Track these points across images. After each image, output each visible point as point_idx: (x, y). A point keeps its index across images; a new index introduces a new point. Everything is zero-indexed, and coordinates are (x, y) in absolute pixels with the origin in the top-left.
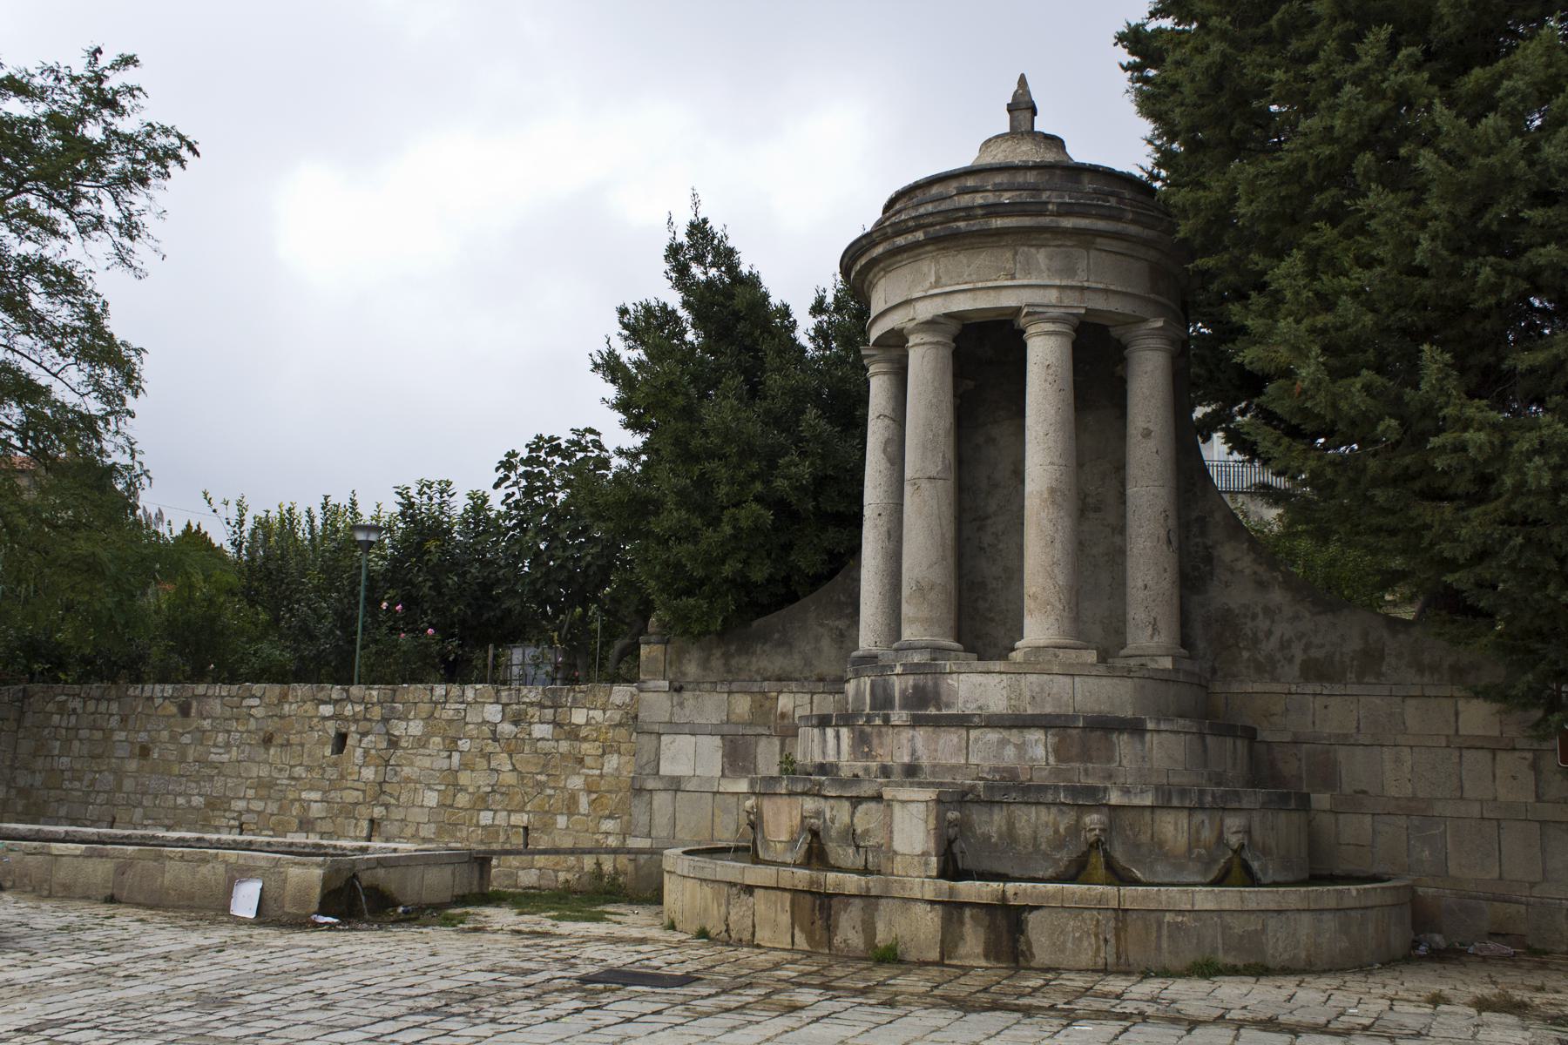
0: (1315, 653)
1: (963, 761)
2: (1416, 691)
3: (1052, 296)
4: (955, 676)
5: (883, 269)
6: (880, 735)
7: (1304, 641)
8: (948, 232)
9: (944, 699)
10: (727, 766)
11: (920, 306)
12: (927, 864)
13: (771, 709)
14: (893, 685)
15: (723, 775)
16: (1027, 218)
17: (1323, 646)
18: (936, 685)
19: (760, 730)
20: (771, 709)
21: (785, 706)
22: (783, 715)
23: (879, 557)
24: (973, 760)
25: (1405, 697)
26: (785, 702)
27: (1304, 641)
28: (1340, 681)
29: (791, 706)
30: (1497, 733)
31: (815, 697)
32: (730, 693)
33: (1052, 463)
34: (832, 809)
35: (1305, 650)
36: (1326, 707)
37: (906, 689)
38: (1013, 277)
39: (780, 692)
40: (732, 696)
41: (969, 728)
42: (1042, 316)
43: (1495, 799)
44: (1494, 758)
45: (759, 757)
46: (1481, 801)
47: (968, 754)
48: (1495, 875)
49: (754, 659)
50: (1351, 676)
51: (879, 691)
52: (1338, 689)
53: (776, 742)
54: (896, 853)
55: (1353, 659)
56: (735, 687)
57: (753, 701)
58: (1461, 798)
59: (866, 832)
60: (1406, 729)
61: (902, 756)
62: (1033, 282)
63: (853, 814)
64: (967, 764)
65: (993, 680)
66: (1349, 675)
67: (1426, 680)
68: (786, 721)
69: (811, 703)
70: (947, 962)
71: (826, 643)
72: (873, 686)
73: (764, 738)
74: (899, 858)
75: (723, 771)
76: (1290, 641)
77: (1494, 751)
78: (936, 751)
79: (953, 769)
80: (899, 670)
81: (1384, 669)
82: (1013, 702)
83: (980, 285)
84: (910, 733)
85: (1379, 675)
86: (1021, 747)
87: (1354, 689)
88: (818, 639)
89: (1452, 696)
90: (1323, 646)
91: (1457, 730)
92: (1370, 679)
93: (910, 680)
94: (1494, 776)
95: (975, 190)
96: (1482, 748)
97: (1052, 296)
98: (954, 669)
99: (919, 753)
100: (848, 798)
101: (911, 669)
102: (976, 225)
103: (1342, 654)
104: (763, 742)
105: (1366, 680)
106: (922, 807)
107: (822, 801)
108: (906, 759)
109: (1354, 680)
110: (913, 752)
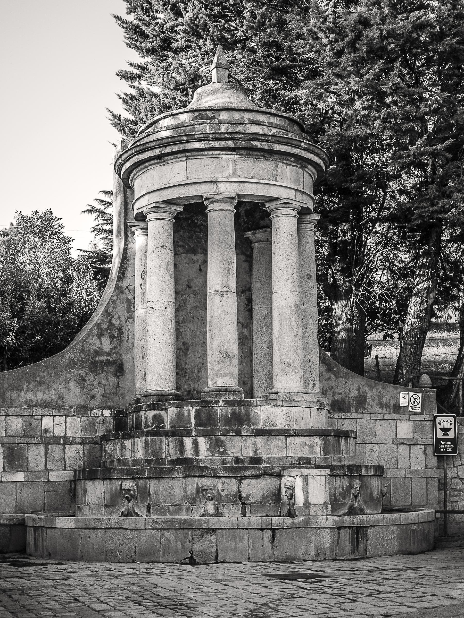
0: (338, 397)
1: (285, 455)
2: (380, 417)
3: (291, 194)
4: (259, 408)
5: (186, 156)
6: (232, 441)
7: (332, 391)
8: (250, 146)
9: (253, 420)
10: (6, 464)
11: (221, 186)
12: (327, 509)
13: (37, 426)
14: (216, 413)
15: (4, 471)
16: (290, 148)
17: (341, 394)
18: (248, 413)
19: (30, 440)
20: (37, 426)
21: (47, 425)
22: (46, 431)
23: (167, 334)
24: (290, 454)
25: (377, 420)
26: (47, 422)
27: (332, 391)
28: (348, 412)
29: (51, 425)
30: (412, 437)
31: (68, 418)
32: (7, 415)
33: (296, 291)
34: (223, 484)
35: (333, 396)
36: (343, 425)
37: (227, 415)
38: (276, 180)
39: (43, 416)
40: (8, 418)
41: (286, 437)
42: (290, 206)
43: (410, 468)
44: (410, 449)
45: (30, 458)
46: (405, 469)
47: (287, 451)
48: (409, 503)
49: (23, 394)
50: (353, 409)
51: (204, 417)
52: (348, 415)
53: (42, 448)
54: (310, 504)
55: (353, 401)
56: (11, 411)
57: (24, 421)
58: (397, 468)
59: (248, 496)
60: (376, 435)
61: (249, 453)
62: (283, 185)
63: (239, 487)
64: (287, 456)
65: (278, 410)
66: (352, 409)
67: (384, 411)
68: (48, 434)
69: (66, 422)
70: (338, 558)
71: (72, 384)
72: (198, 414)
73: (33, 445)
74: (312, 507)
75: (4, 468)
76: (326, 391)
77: (410, 445)
78: (270, 449)
79: (280, 458)
80: (221, 403)
81: (367, 406)
82: (288, 423)
83: (261, 181)
84: (253, 439)
85: (364, 409)
86: (311, 446)
87: (355, 416)
88: (67, 381)
89: (395, 420)
90: (341, 394)
91: (396, 436)
92: (361, 411)
93: (230, 409)
94: (410, 457)
95: (259, 123)
96: (406, 444)
97: (291, 194)
98: (259, 403)
99: (260, 451)
100: (235, 477)
101: (228, 403)
102: (265, 146)
103: (349, 398)
104: (32, 449)
105: (359, 411)
106: (323, 478)
107: (216, 480)
108: (251, 455)
109: (354, 411)
110: (256, 451)
